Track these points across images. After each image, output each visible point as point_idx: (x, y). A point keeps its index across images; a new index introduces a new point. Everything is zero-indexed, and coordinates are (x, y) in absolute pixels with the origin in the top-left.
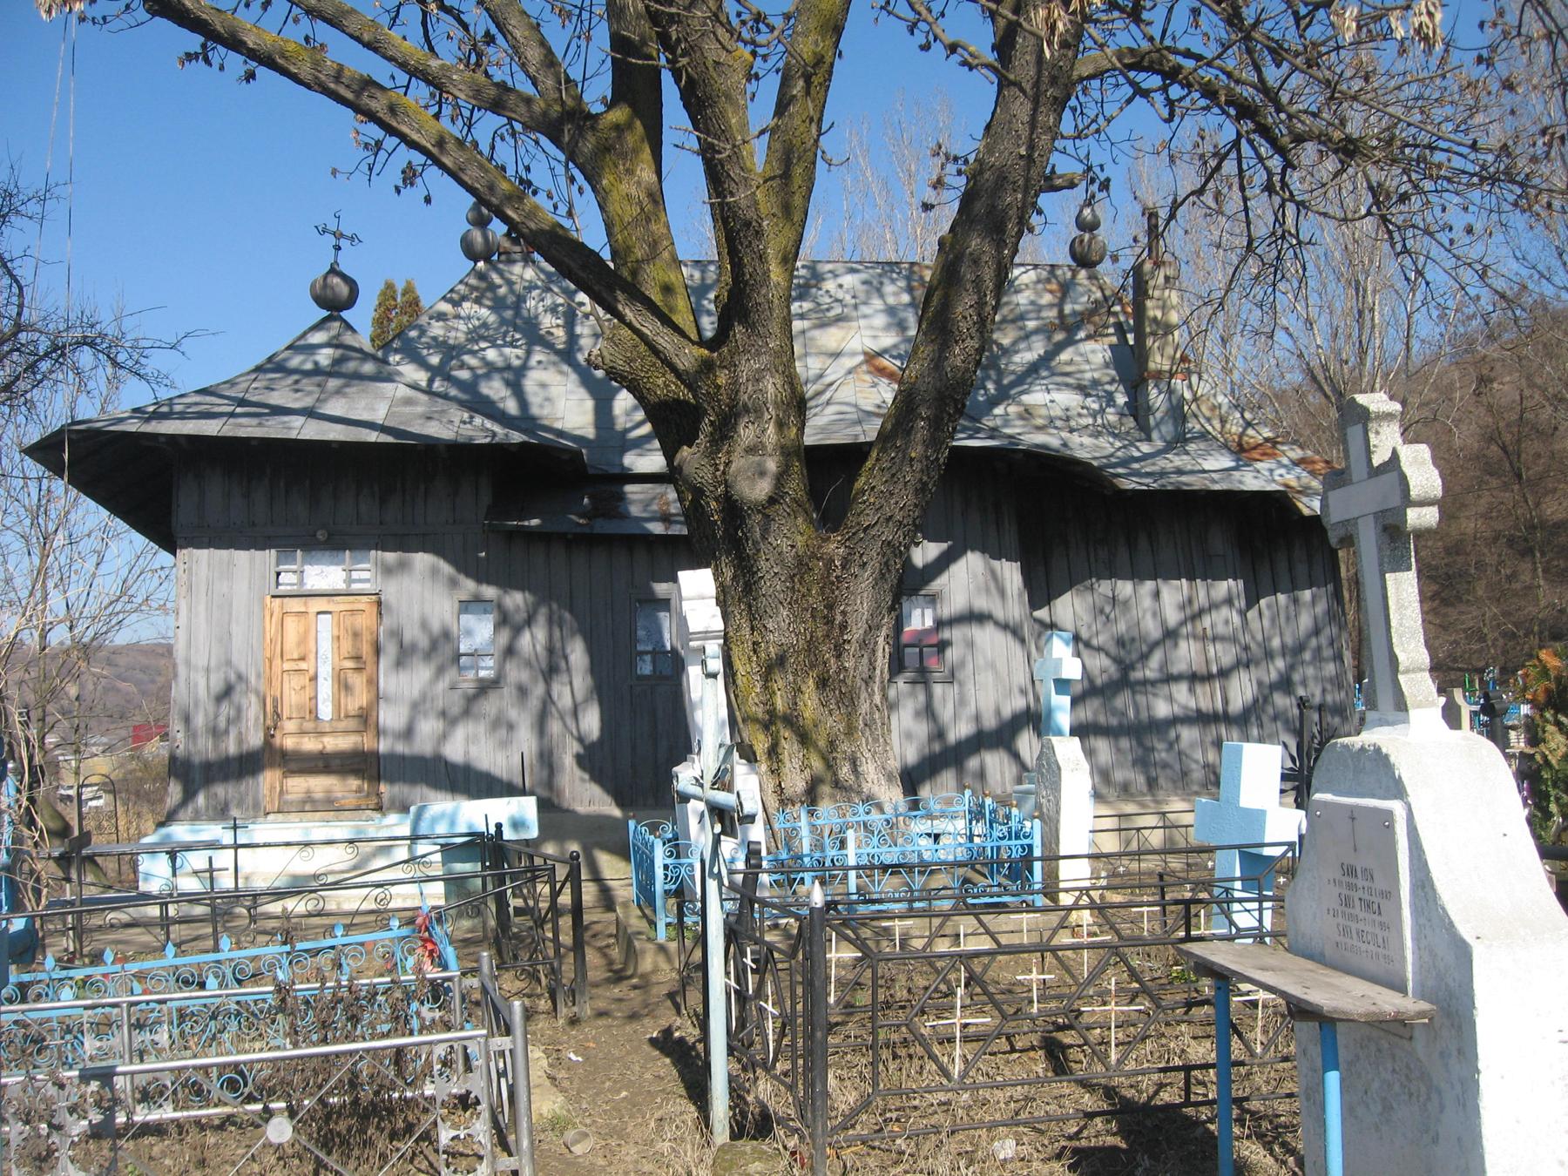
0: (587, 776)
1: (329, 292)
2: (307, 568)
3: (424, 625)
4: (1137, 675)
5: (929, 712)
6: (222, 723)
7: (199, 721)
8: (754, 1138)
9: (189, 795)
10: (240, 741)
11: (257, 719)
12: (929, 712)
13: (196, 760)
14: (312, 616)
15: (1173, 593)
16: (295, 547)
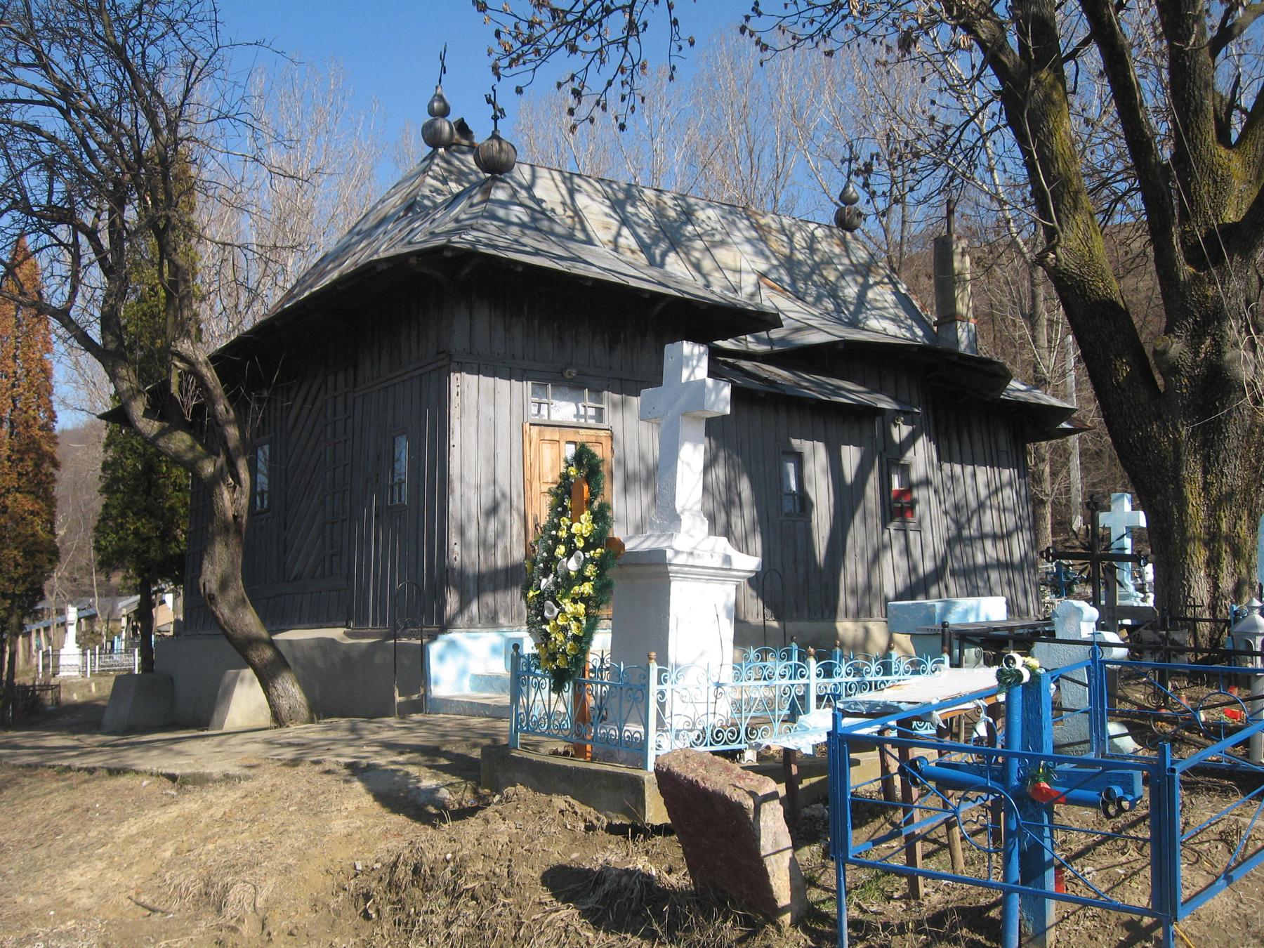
0: (755, 594)
1: (503, 156)
2: (556, 402)
3: (642, 458)
4: (966, 533)
5: (907, 551)
6: (491, 535)
7: (472, 533)
8: (584, 914)
9: (464, 605)
10: (505, 556)
11: (519, 535)
12: (907, 551)
13: (471, 570)
14: (562, 443)
15: (983, 474)
16: (548, 381)
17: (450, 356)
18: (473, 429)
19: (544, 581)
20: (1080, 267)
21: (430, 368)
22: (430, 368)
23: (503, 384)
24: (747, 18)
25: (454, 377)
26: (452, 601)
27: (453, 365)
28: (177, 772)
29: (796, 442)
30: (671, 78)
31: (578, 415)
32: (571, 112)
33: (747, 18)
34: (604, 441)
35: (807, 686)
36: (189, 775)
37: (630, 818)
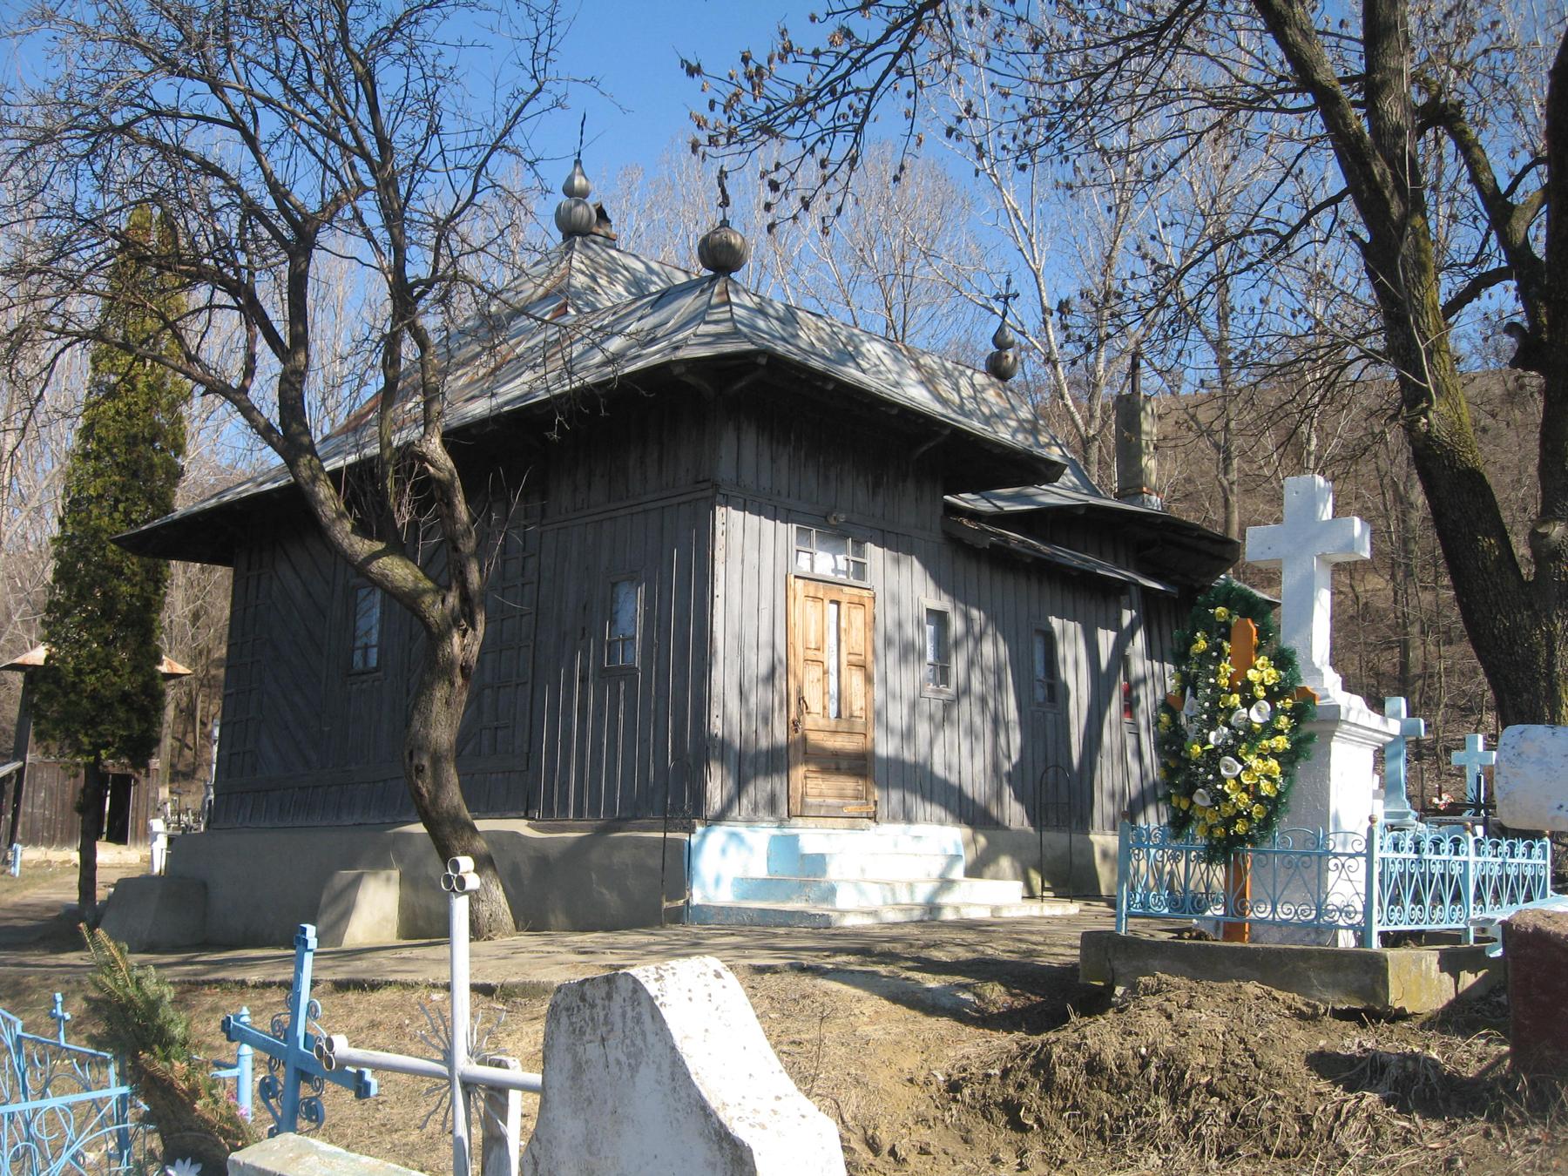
14: (826, 602)
17: (716, 486)
18: (736, 577)
19: (1212, 735)
20: (1451, 435)
21: (684, 498)
22: (684, 498)
23: (768, 524)
24: (959, 120)
25: (720, 511)
26: (716, 789)
27: (719, 498)
28: (492, 981)
29: (1056, 623)
30: (896, 179)
31: (836, 571)
32: (768, 207)
33: (959, 120)
34: (866, 602)
35: (1466, 863)
36: (516, 986)
37: (1362, 999)
